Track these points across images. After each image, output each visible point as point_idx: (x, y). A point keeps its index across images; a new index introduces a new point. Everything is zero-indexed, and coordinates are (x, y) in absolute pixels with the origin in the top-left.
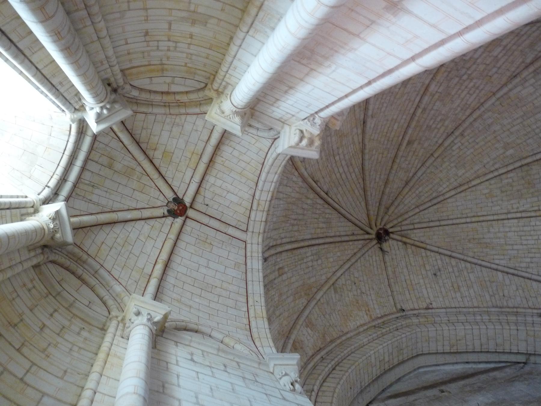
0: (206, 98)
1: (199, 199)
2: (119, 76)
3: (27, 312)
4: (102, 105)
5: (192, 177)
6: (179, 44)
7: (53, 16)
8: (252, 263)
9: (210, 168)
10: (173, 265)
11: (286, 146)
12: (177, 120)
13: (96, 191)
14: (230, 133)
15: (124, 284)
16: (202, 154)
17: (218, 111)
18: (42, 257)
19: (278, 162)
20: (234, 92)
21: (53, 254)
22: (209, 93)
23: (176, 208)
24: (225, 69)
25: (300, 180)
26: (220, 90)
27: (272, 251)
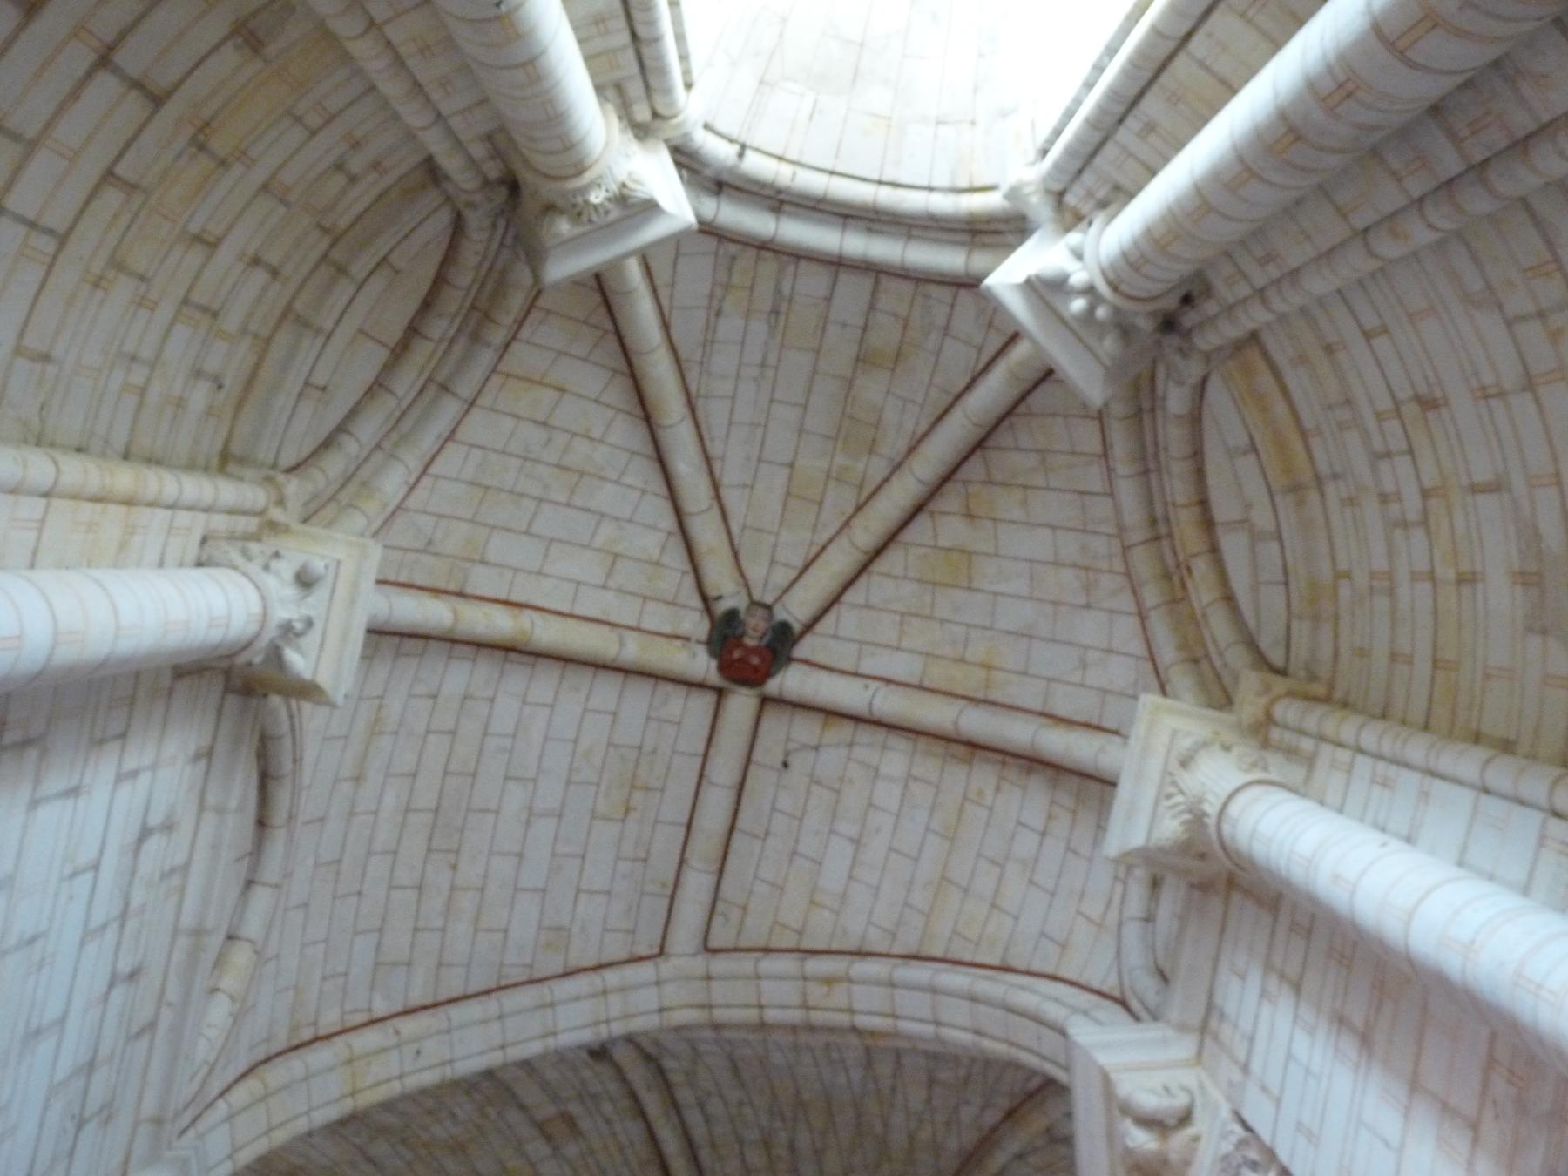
0: (1227, 680)
1: (805, 729)
2: (1230, 331)
3: (259, 175)
4: (1103, 288)
5: (888, 681)
6: (1418, 535)
7: (1413, 65)
8: (578, 998)
9: (939, 748)
10: (517, 677)
11: (1104, 1059)
12: (1107, 582)
13: (759, 328)
14: (1104, 808)
15: (412, 502)
16: (994, 704)
17: (1187, 743)
18: (470, 185)
19: (1027, 1033)
20: (1282, 795)
21: (487, 223)
22: (1250, 689)
23: (750, 642)
24: (1369, 739)
25: (969, 1138)
26: (1275, 734)
27: (639, 1076)
